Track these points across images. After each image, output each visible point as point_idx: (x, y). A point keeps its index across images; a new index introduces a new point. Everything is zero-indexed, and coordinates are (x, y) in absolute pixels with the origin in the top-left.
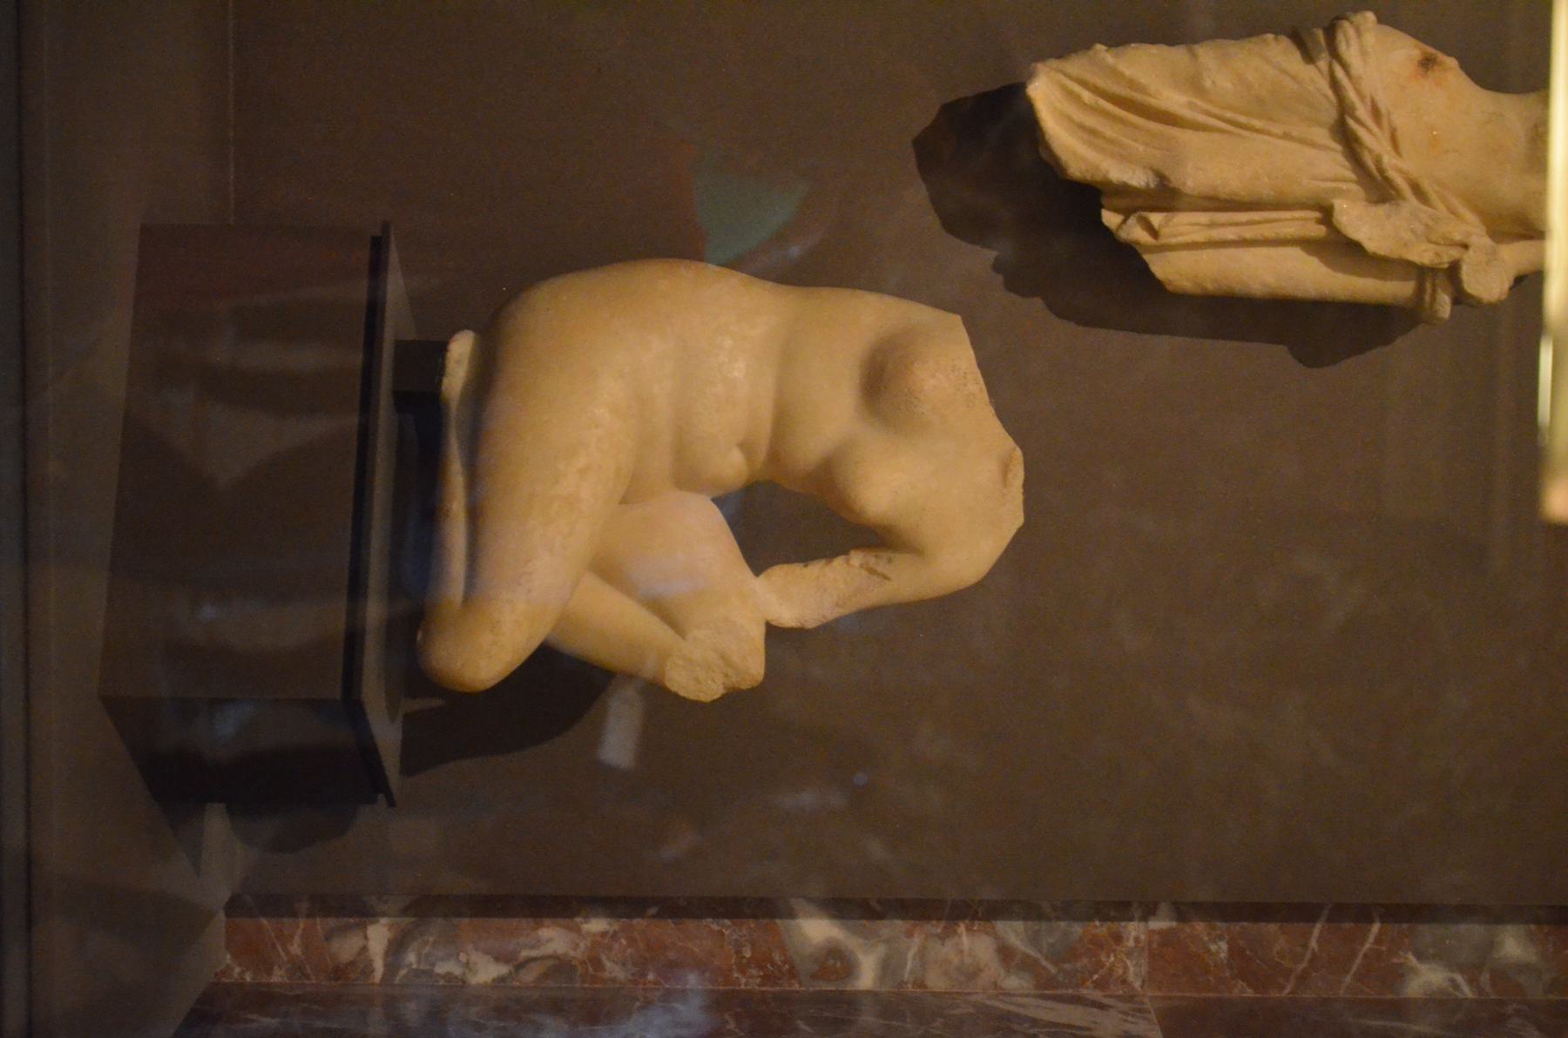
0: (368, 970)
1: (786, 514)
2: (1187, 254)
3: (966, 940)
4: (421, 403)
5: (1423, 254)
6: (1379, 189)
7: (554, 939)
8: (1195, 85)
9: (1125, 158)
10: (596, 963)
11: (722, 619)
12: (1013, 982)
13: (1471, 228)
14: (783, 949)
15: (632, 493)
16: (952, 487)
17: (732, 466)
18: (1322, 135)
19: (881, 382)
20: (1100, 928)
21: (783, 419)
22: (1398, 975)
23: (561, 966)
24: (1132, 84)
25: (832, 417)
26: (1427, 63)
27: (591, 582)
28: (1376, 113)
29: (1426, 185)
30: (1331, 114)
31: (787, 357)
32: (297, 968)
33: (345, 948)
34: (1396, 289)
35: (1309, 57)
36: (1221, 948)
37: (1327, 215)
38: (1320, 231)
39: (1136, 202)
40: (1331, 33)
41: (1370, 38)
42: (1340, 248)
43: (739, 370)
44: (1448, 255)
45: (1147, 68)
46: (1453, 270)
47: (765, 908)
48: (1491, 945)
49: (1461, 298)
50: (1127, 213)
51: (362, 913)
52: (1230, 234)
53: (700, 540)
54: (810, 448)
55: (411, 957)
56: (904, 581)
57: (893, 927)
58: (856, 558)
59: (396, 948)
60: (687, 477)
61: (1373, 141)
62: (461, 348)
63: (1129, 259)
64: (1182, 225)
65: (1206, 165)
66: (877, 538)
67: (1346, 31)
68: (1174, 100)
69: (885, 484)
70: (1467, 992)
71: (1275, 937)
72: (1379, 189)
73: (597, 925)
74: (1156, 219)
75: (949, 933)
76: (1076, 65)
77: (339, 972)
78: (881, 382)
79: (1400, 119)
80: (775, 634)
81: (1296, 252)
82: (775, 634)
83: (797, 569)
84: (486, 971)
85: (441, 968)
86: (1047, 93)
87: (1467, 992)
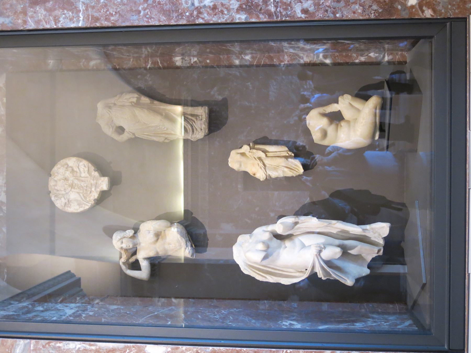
0: (387, 54)
1: (336, 118)
2: (283, 150)
3: (308, 60)
4: (382, 129)
5: (254, 151)
6: (260, 159)
7: (363, 59)
8: (284, 172)
9: (292, 162)
10: (357, 56)
11: (345, 104)
12: (302, 55)
13: (247, 153)
14: (332, 59)
15: (356, 120)
16: (315, 122)
17: (343, 123)
18: (267, 165)
19: (325, 134)
20: (290, 62)
21: (337, 130)
22: (252, 58)
23: (362, 55)
24: (291, 171)
25: (331, 130)
26: (254, 174)
27: (361, 109)
28: (261, 168)
29: (254, 159)
30: (266, 168)
31: (336, 137)
32: (397, 54)
33: (391, 57)
34: (257, 146)
35: (269, 175)
36: (275, 60)
37: (266, 156)
38: (267, 153)
39: (290, 157)
40: (266, 178)
41: (262, 177)
42: (265, 152)
43: (342, 136)
44: (252, 151)
45: (289, 174)
46: (250, 149)
47: (335, 64)
48: (240, 62)
49: (249, 145)
50: (291, 156)
51: (389, 62)
52: (278, 153)
53: (347, 114)
54: (333, 127)
55: (382, 56)
56: (321, 110)
57: (318, 62)
58: (327, 112)
59: (384, 57)
60: (348, 122)
61: (261, 164)
62: (377, 138)
63: (290, 150)
64: (285, 154)
65: (282, 162)
66: (324, 115)
67: (265, 178)
68: (286, 170)
69: (324, 122)
70: (243, 56)
71: (268, 62)
72: (260, 159)
73: (357, 61)
74: (287, 155)
75: (310, 61)
76: (298, 174)
77: (391, 54)
78: (325, 134)
79: (258, 167)
80: (337, 102)
81: (270, 151)
82: (337, 102)
83: (335, 111)
84: (372, 55)
85: (378, 55)
86: (301, 170)
87: (243, 56)
